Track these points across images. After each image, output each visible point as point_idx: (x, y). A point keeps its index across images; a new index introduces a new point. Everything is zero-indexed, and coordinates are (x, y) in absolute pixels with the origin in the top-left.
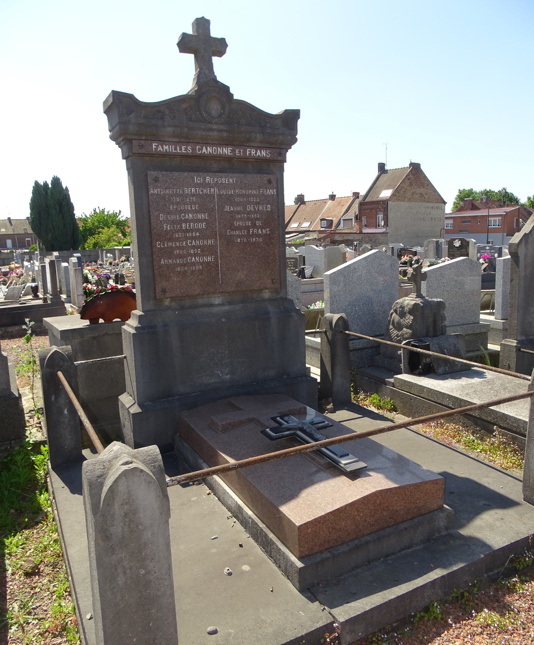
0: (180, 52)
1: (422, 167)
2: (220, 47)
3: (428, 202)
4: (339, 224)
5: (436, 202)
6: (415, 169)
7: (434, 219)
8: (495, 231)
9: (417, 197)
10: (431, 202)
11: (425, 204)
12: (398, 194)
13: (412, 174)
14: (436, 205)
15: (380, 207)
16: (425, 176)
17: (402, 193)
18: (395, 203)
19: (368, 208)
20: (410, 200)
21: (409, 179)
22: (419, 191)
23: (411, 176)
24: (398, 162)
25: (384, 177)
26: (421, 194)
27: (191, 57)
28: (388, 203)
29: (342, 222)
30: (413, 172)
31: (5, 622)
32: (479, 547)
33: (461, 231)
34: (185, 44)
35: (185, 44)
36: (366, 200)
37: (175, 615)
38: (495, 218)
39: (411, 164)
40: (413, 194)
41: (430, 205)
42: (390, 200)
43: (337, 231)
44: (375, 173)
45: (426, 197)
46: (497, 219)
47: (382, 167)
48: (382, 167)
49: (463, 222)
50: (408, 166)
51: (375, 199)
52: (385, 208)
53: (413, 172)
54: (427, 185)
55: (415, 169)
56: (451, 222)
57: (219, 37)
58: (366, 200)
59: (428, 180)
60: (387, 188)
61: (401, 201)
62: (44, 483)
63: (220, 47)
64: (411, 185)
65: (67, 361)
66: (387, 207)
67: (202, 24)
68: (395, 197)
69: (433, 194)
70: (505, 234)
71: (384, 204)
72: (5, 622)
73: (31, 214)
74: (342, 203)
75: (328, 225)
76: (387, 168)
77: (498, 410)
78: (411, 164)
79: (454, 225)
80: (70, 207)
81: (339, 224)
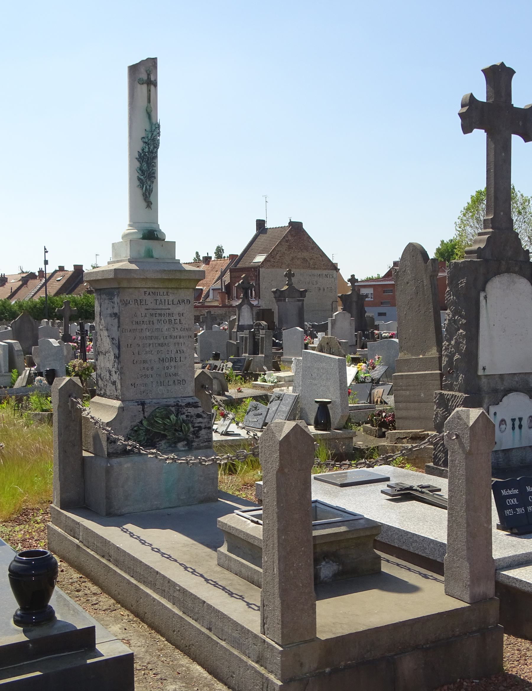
1: (305, 227)
3: (314, 268)
4: (207, 295)
5: (326, 269)
6: (296, 228)
7: (322, 289)
9: (299, 262)
10: (317, 269)
11: (310, 271)
12: (272, 260)
13: (292, 235)
14: (325, 272)
15: (252, 275)
17: (278, 258)
19: (241, 274)
21: (287, 241)
22: (300, 255)
23: (290, 238)
24: (277, 221)
25: (263, 237)
28: (259, 270)
29: (211, 292)
30: (293, 233)
33: (382, 303)
36: (238, 266)
39: (291, 223)
40: (293, 259)
42: (262, 267)
43: (206, 304)
44: (253, 231)
47: (261, 224)
48: (261, 224)
49: (384, 292)
50: (288, 225)
51: (247, 265)
52: (257, 276)
53: (293, 233)
54: (312, 249)
55: (296, 228)
56: (370, 291)
57: (459, 121)
58: (238, 266)
60: (261, 253)
61: (278, 267)
64: (290, 248)
66: (259, 275)
68: (269, 264)
69: (321, 258)
71: (256, 270)
74: (217, 267)
75: (197, 295)
76: (268, 225)
77: (511, 575)
78: (291, 223)
79: (375, 295)
80: (319, 408)
81: (207, 295)
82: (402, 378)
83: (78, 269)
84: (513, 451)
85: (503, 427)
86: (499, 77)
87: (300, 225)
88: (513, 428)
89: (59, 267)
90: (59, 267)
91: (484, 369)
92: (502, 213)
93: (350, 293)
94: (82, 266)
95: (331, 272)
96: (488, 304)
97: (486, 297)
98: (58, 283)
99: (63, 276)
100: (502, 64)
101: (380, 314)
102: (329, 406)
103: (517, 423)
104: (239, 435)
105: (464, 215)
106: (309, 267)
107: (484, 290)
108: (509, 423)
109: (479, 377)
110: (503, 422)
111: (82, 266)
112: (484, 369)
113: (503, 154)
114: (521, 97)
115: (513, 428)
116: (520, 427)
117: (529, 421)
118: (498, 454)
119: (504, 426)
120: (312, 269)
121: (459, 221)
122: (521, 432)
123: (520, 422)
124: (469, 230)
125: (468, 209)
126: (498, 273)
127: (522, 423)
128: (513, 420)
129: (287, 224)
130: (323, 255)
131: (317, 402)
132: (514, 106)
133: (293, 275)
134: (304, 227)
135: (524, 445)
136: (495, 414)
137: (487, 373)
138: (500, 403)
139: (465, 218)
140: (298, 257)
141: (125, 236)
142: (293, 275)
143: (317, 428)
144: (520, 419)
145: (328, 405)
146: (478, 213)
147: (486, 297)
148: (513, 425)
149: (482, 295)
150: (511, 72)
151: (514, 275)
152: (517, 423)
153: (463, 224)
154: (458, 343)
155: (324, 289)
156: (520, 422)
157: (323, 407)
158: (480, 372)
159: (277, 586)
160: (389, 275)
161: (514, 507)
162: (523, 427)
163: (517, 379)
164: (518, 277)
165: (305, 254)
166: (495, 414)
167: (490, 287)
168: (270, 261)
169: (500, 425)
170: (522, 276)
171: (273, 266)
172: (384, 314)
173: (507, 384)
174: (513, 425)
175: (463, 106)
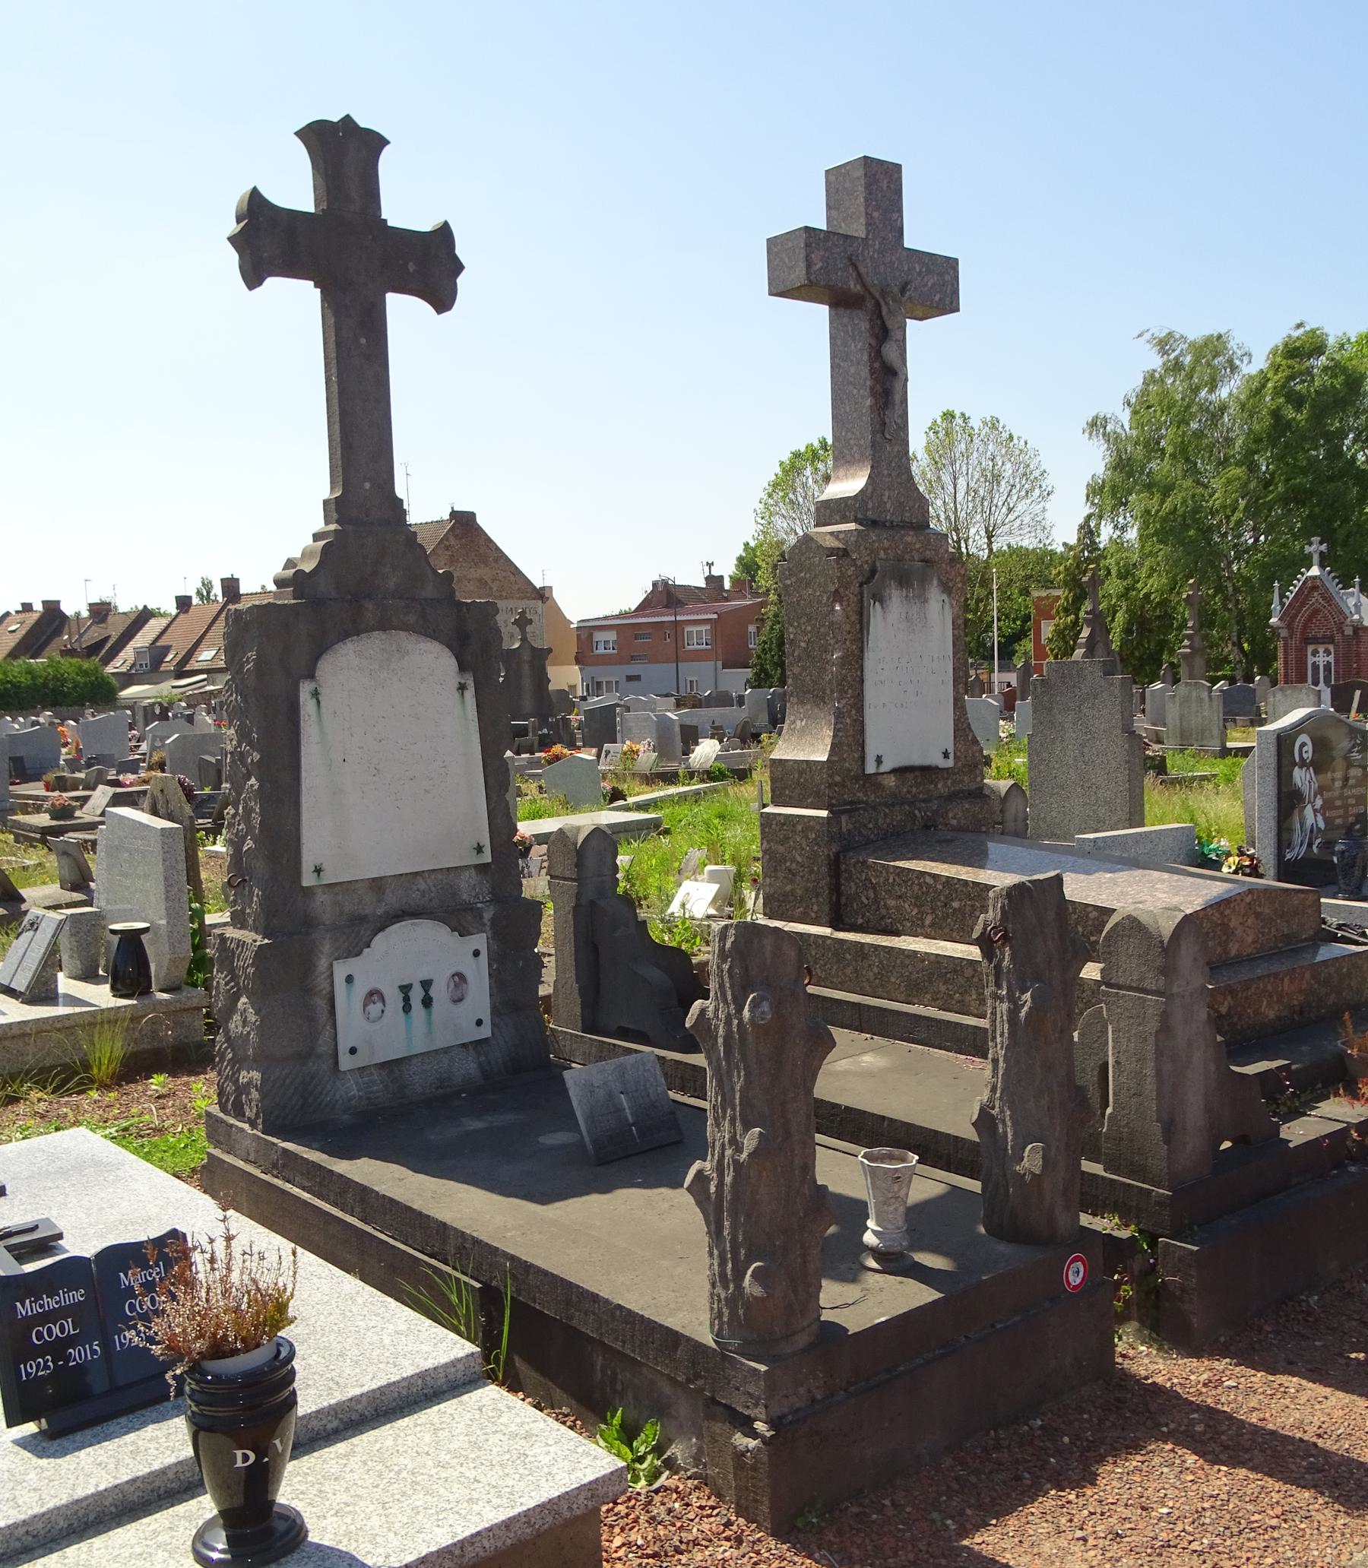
0: (772, 242)
1: (479, 520)
2: (936, 286)
8: (698, 656)
13: (456, 536)
16: (490, 541)
21: (447, 548)
26: (480, 580)
27: (917, 236)
30: (458, 532)
31: (284, 1371)
33: (632, 658)
38: (699, 628)
39: (454, 514)
45: (495, 586)
46: (703, 628)
53: (458, 532)
54: (496, 561)
56: (612, 636)
57: (234, 256)
62: (1252, 861)
63: (936, 286)
67: (873, 187)
69: (512, 578)
70: (720, 663)
72: (284, 1371)
73: (294, 581)
78: (454, 514)
83: (52, 609)
84: (414, 1061)
85: (375, 1008)
86: (344, 151)
87: (471, 516)
88: (407, 1008)
89: (23, 605)
90: (23, 605)
91: (318, 871)
92: (367, 485)
93: (516, 646)
94: (58, 602)
96: (323, 710)
97: (316, 694)
98: (11, 636)
99: (21, 623)
100: (348, 119)
101: (630, 678)
102: (144, 938)
103: (416, 996)
105: (770, 496)
107: (311, 676)
108: (394, 998)
109: (308, 892)
110: (375, 997)
111: (58, 602)
112: (318, 871)
113: (363, 341)
114: (405, 205)
115: (407, 1008)
116: (427, 1002)
117: (452, 985)
118: (371, 1074)
119: (379, 1006)
121: (762, 506)
122: (430, 1014)
123: (426, 992)
124: (780, 523)
125: (775, 485)
126: (354, 629)
127: (432, 993)
128: (406, 989)
129: (447, 517)
130: (517, 572)
131: (113, 932)
132: (390, 224)
134: (479, 521)
135: (440, 1043)
136: (349, 979)
137: (328, 878)
138: (366, 951)
139: (771, 501)
143: (117, 992)
144: (426, 984)
145: (142, 937)
146: (795, 492)
147: (316, 694)
148: (407, 1000)
149: (305, 689)
150: (376, 143)
151: (403, 634)
152: (416, 996)
153: (768, 513)
154: (248, 811)
156: (426, 992)
157: (132, 941)
158: (308, 880)
160: (645, 606)
161: (59, 1348)
162: (434, 1004)
163: (423, 886)
164: (414, 637)
165: (483, 572)
166: (349, 979)
167: (326, 667)
169: (365, 1005)
170: (426, 636)
172: (638, 678)
173: (392, 900)
174: (407, 1000)
175: (238, 221)
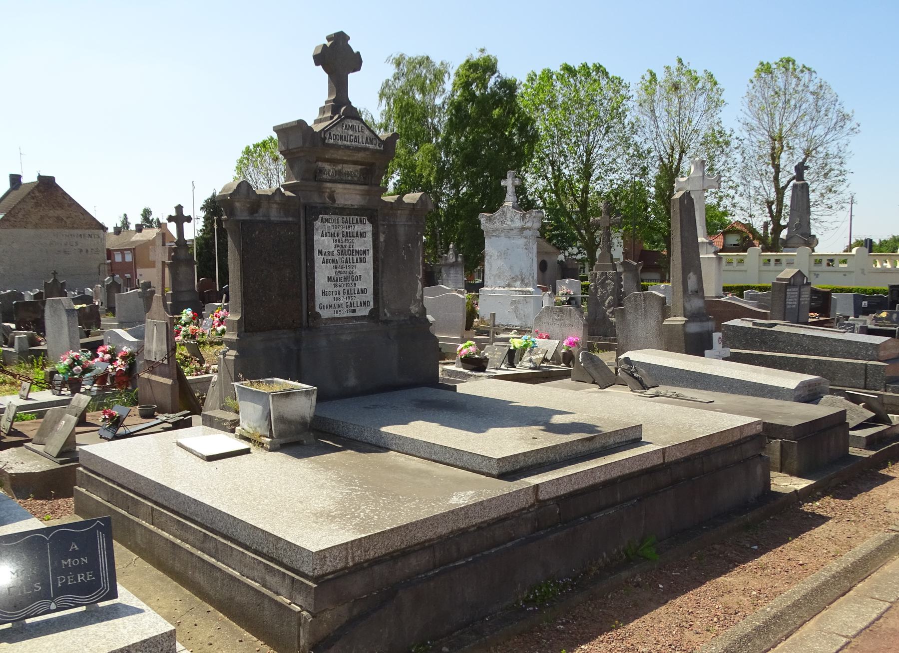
2: (355, 62)
3: (73, 228)
7: (84, 251)
12: (13, 219)
13: (40, 191)
14: (88, 232)
18: (8, 231)
20: (36, 226)
22: (52, 213)
26: (58, 218)
27: (320, 67)
32: (824, 191)
34: (323, 58)
35: (323, 58)
37: (555, 432)
40: (42, 218)
41: (76, 232)
44: (6, 186)
45: (68, 221)
53: (41, 188)
59: (71, 199)
61: (21, 227)
64: (37, 205)
65: (88, 334)
68: (7, 223)
69: (81, 217)
78: (40, 177)
82: (856, 354)
95: (96, 231)
104: (631, 438)
106: (65, 227)
120: (69, 228)
133: (807, 168)
140: (50, 215)
141: (326, 102)
142: (807, 168)
155: (87, 251)
159: (658, 611)
165: (59, 212)
168: (8, 220)
171: (14, 227)
